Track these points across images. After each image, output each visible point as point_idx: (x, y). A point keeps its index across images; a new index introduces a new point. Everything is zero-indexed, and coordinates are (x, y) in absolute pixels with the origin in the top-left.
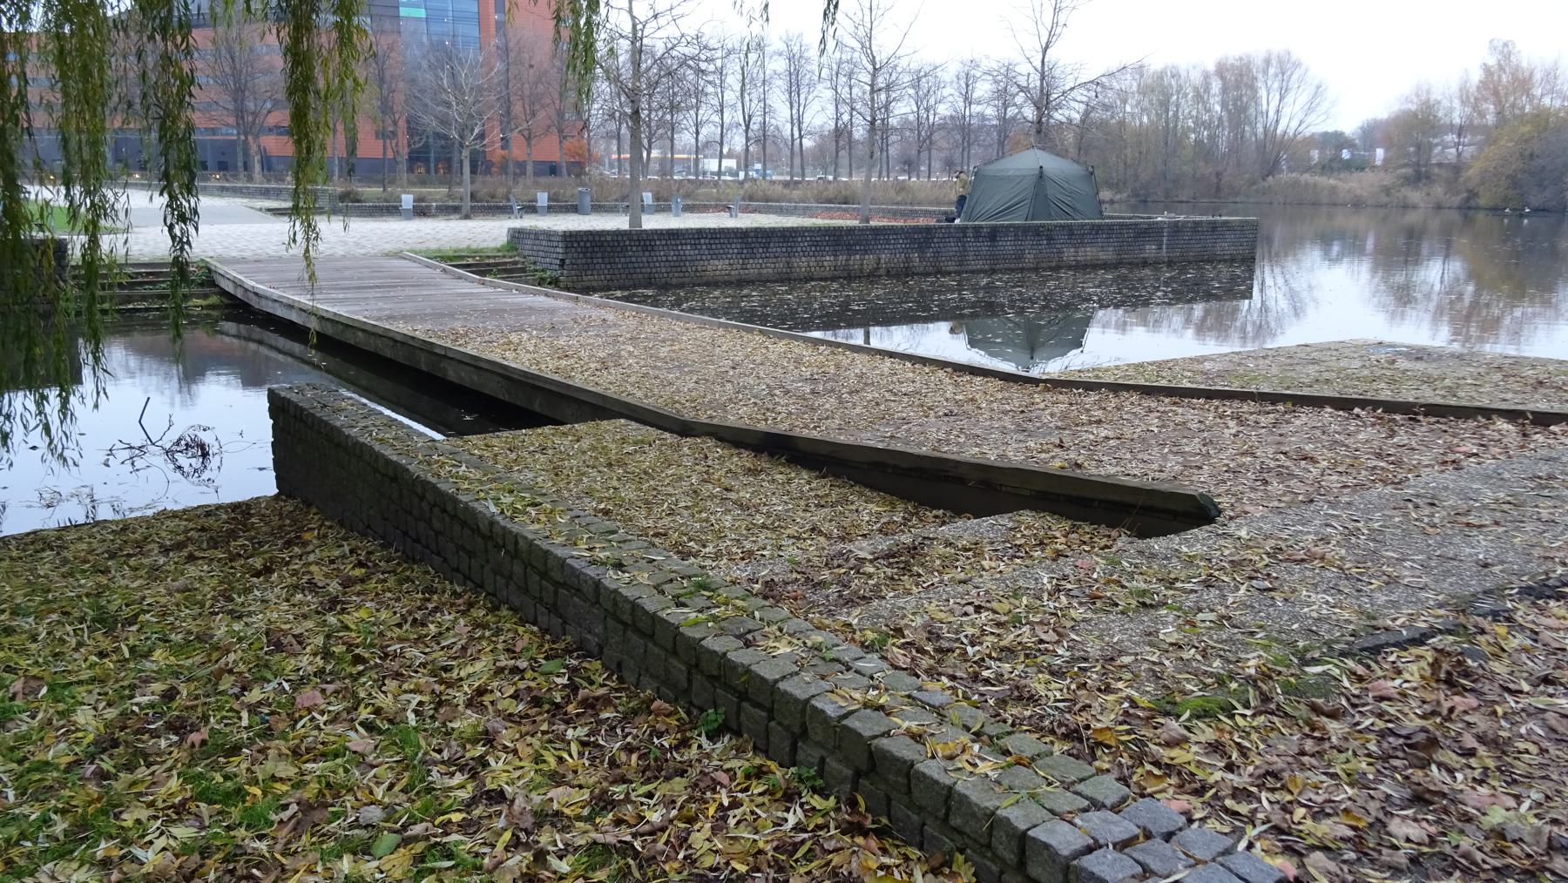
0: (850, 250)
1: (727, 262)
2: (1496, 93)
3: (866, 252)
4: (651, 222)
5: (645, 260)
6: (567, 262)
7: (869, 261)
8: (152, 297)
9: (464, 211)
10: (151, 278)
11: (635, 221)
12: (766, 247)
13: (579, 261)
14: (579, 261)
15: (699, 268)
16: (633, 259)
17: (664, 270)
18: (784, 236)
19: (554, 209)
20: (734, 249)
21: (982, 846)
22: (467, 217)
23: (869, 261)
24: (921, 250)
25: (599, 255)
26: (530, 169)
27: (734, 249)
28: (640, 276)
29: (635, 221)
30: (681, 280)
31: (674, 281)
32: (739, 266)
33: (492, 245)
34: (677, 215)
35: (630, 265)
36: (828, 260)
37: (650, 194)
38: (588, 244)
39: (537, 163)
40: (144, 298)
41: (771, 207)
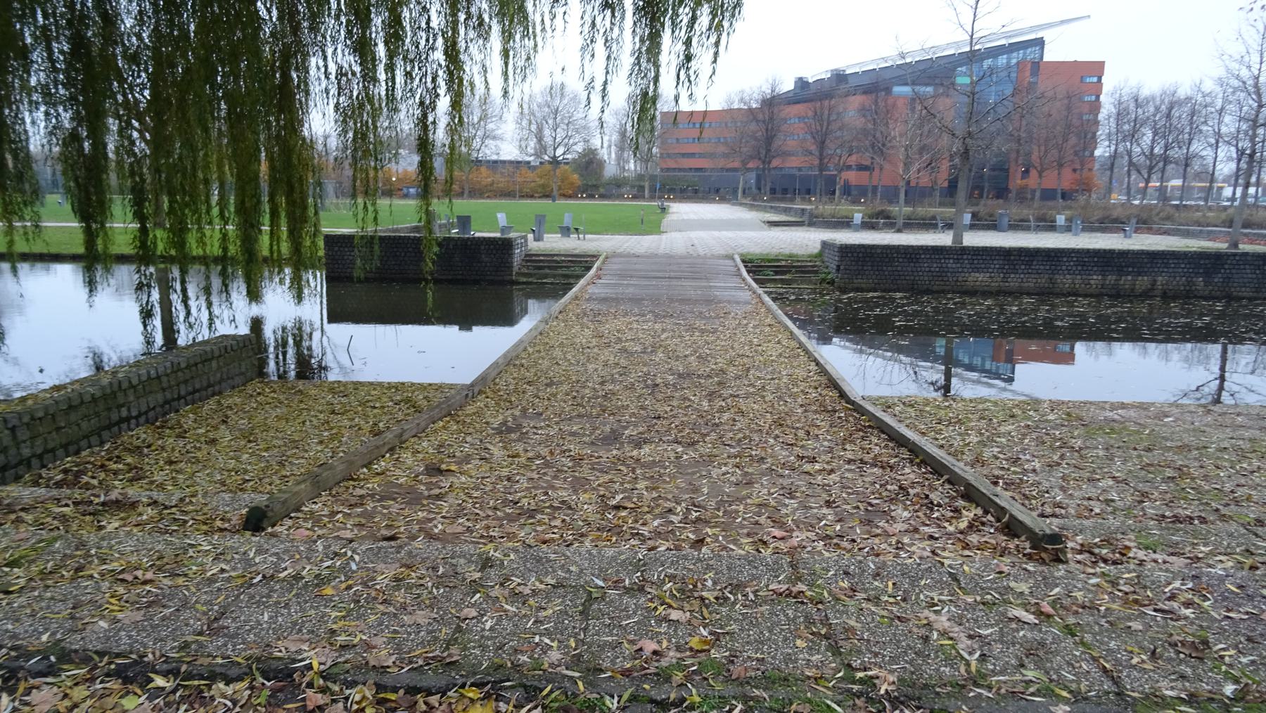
0: (1121, 271)
1: (988, 275)
2: (1136, 100)
3: (1139, 274)
4: (974, 239)
5: (909, 269)
6: (842, 267)
7: (1143, 282)
8: (559, 275)
9: (897, 227)
10: (569, 264)
11: (957, 238)
12: (1029, 263)
13: (852, 267)
14: (852, 267)
15: (960, 279)
16: (899, 268)
17: (926, 278)
18: (1049, 256)
19: (868, 226)
20: (997, 263)
21: (821, 678)
22: (899, 231)
23: (1143, 282)
24: (1207, 274)
25: (869, 264)
26: (1038, 194)
27: (997, 263)
28: (904, 282)
29: (957, 238)
30: (941, 288)
31: (935, 288)
32: (999, 279)
33: (800, 253)
34: (1076, 234)
35: (896, 273)
36: (1095, 279)
37: (504, 215)
38: (861, 255)
39: (1043, 191)
40: (554, 276)
41: (1179, 230)
